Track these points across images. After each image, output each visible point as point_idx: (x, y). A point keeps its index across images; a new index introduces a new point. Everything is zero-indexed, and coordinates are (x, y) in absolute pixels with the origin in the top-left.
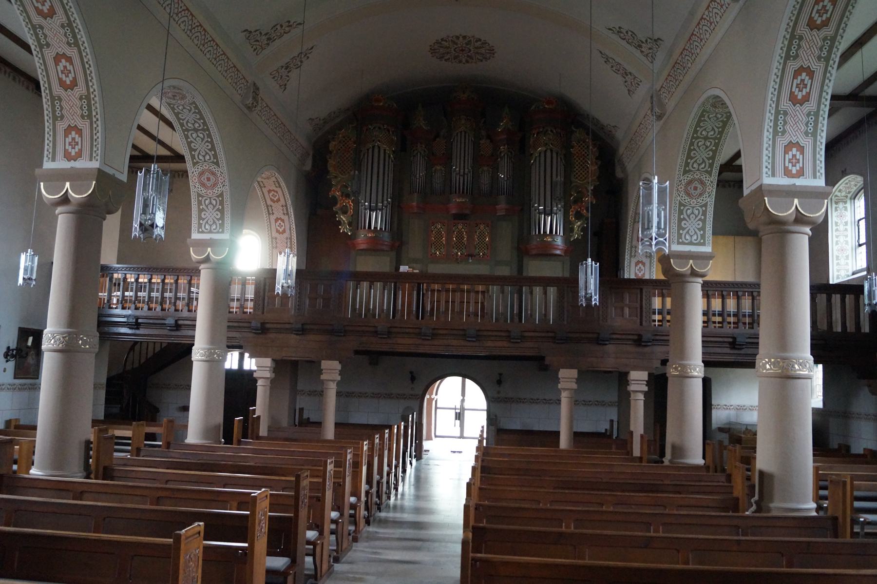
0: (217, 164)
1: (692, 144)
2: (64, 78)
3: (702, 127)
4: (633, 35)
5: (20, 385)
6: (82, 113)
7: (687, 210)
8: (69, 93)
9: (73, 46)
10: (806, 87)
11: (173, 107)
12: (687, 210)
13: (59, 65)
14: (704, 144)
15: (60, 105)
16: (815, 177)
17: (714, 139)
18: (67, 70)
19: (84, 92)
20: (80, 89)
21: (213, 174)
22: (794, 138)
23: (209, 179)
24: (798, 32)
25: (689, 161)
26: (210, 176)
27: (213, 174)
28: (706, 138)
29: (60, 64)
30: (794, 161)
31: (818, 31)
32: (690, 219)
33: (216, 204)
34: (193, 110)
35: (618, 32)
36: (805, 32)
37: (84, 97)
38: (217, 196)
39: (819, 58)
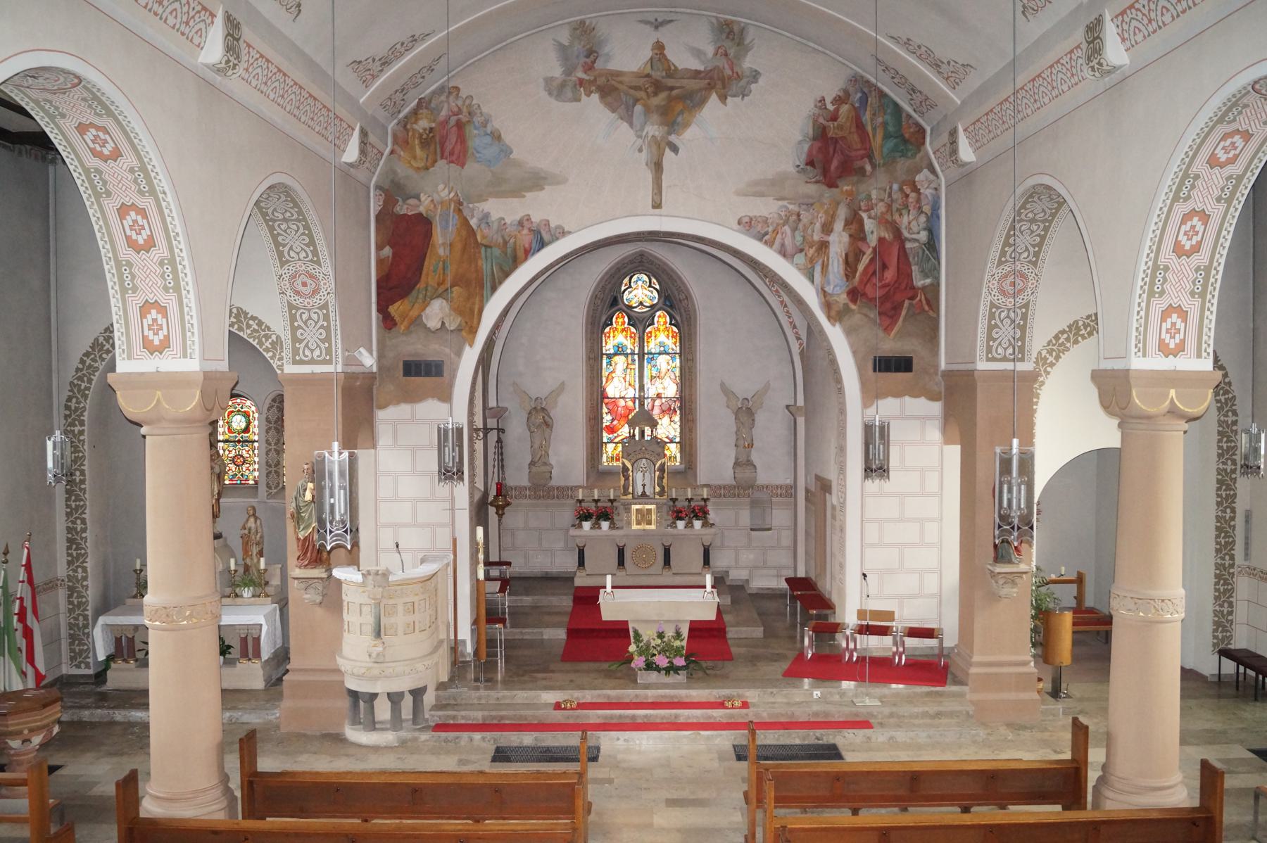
0: (318, 263)
1: (1013, 228)
2: (134, 237)
3: (1036, 235)
4: (929, 52)
5: (45, 584)
6: (165, 284)
7: (1000, 313)
8: (144, 256)
9: (171, 291)
10: (1197, 233)
11: (273, 225)
12: (1000, 313)
13: (125, 219)
14: (1029, 229)
15: (131, 273)
16: (1199, 356)
17: (1044, 221)
18: (139, 225)
19: (166, 255)
20: (160, 251)
21: (312, 277)
22: (1176, 301)
23: (304, 284)
24: (1194, 169)
25: (1006, 249)
26: (305, 280)
27: (312, 277)
28: (1033, 221)
29: (128, 217)
30: (1173, 331)
31: (1221, 168)
32: (1009, 340)
33: (318, 320)
34: (301, 230)
35: (905, 43)
36: (1213, 206)
37: (166, 262)
38: (318, 308)
39: (1219, 200)
